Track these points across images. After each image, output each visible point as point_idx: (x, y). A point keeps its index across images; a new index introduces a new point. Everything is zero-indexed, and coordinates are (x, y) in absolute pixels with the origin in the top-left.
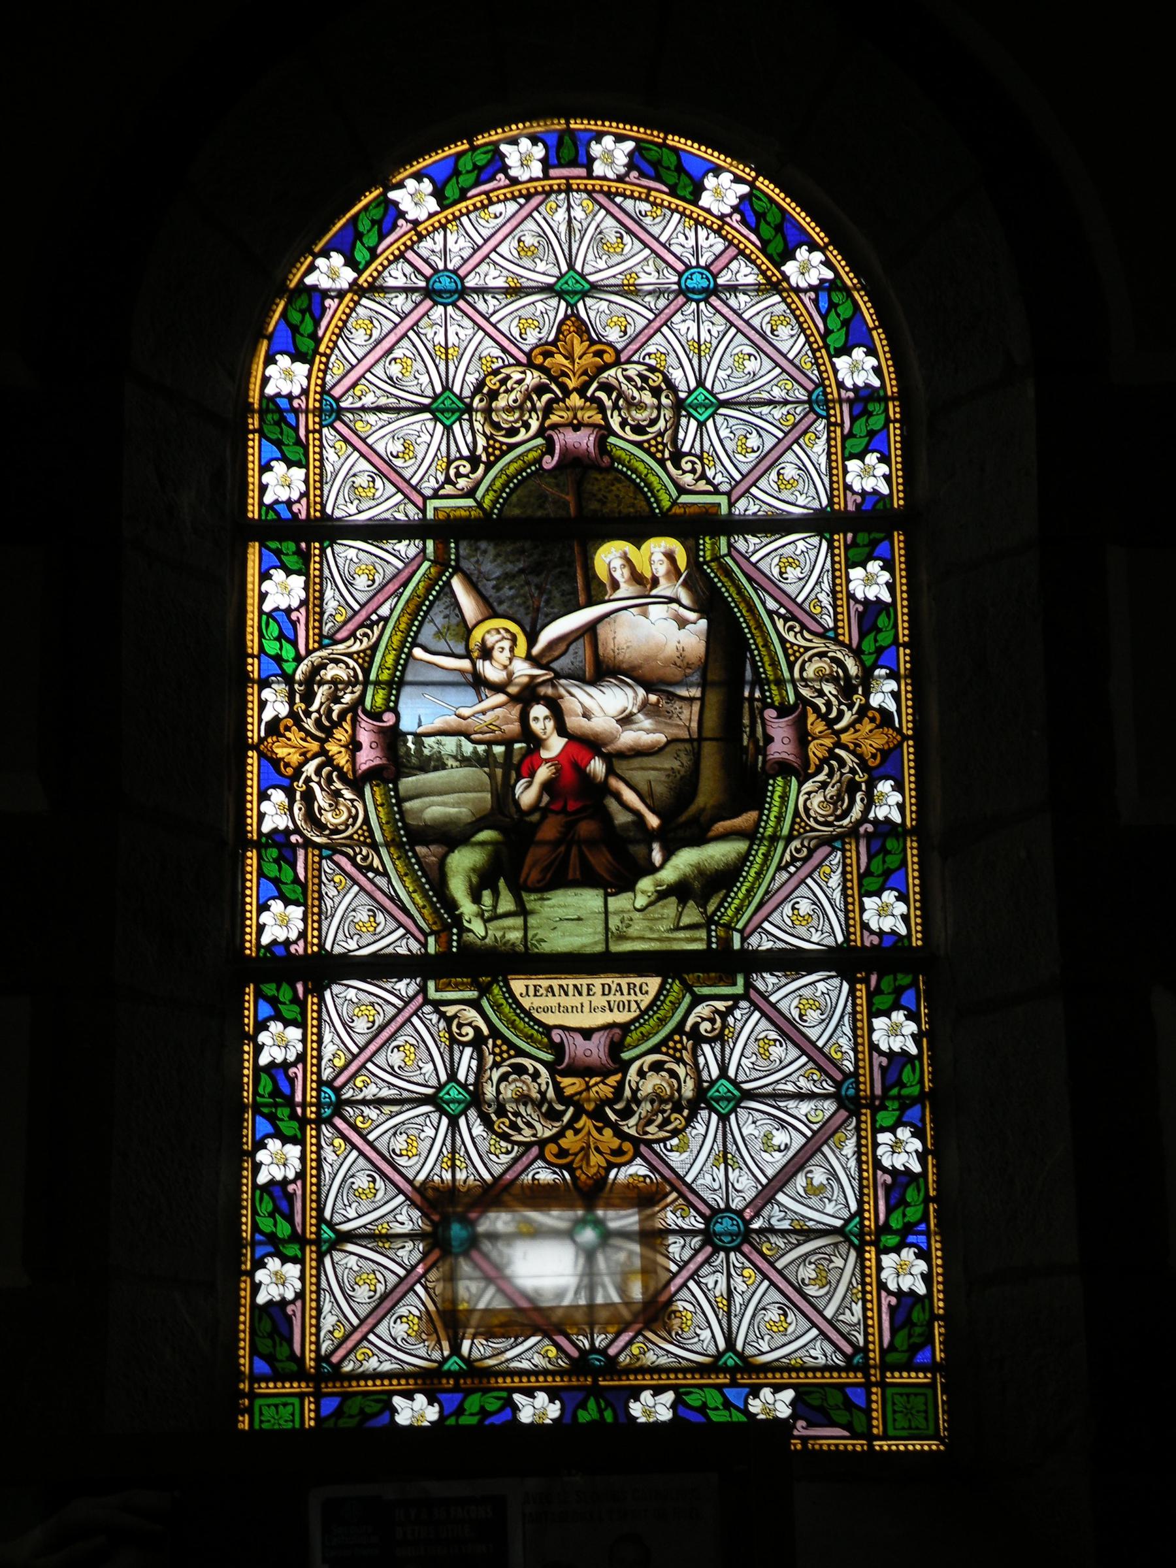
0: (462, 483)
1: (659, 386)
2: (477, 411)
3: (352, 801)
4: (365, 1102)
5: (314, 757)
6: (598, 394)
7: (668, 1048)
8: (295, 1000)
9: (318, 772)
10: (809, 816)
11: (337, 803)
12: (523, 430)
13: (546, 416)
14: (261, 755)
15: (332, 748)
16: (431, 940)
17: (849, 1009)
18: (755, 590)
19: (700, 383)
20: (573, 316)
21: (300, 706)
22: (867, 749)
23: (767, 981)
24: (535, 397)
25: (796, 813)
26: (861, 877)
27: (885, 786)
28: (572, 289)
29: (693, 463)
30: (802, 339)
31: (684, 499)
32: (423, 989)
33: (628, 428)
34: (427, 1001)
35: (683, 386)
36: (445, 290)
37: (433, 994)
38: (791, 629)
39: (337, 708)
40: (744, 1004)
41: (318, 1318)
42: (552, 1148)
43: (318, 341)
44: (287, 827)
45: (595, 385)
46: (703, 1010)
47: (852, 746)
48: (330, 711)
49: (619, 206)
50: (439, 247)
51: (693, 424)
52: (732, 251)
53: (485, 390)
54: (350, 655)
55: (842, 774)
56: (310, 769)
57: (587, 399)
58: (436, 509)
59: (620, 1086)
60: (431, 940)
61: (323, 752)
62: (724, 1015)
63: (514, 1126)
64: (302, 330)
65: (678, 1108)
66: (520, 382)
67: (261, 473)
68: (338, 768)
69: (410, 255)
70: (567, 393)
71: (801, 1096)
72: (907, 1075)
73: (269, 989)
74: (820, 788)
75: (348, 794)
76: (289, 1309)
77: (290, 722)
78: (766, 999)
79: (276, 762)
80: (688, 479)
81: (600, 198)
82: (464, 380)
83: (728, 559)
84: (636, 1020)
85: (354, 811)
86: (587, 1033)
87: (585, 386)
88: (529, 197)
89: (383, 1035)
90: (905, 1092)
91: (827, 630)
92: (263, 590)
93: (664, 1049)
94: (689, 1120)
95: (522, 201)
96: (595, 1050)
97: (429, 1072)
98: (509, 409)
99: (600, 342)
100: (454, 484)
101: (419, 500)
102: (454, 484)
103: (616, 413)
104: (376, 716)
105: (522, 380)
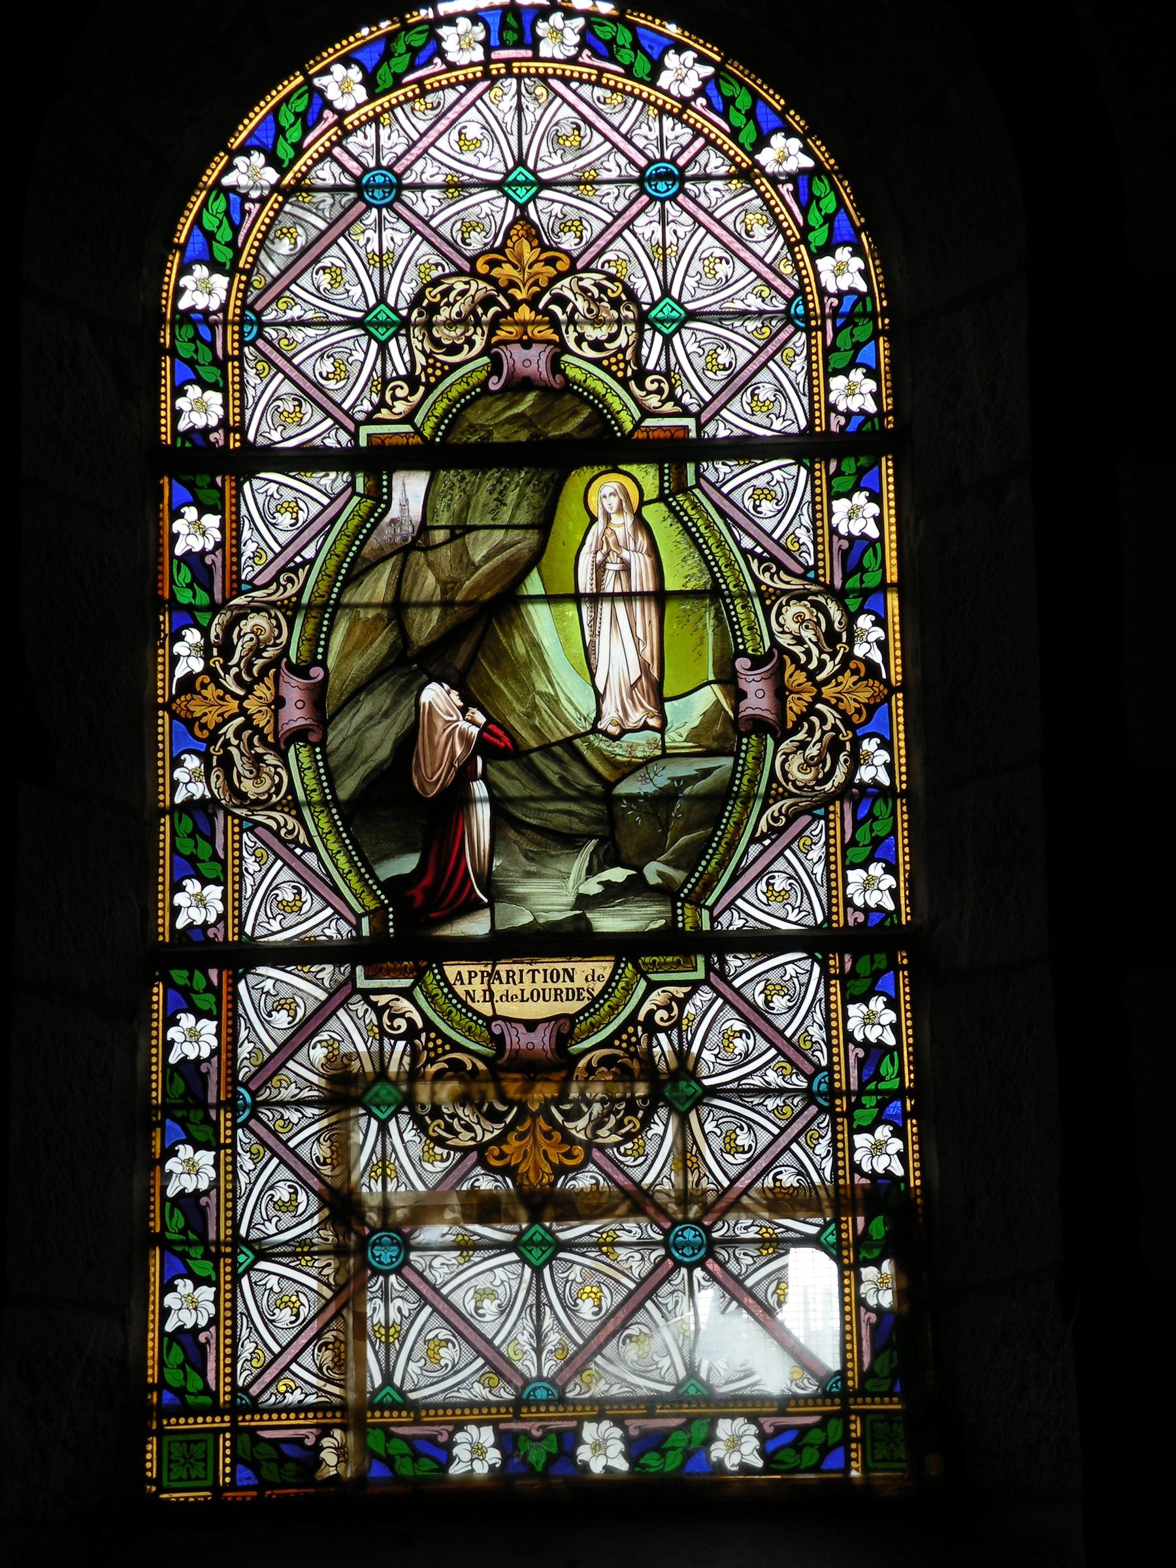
0: (401, 407)
1: (433, 1120)
2: (415, 326)
3: (276, 767)
4: (284, 1104)
5: (233, 717)
6: (504, 1108)
7: (622, 1041)
8: (210, 988)
9: (238, 733)
10: (787, 780)
11: (259, 770)
12: (466, 347)
13: (492, 333)
14: (174, 716)
15: (251, 705)
16: (365, 921)
17: (248, 413)
18: (329, 875)
19: (666, 292)
20: (522, 216)
21: (217, 662)
22: (850, 706)
23: (339, 439)
24: (480, 311)
25: (773, 777)
26: (845, 848)
27: (869, 745)
28: (521, 180)
29: (392, 1027)
30: (781, 240)
31: (649, 422)
32: (700, 427)
33: (585, 345)
34: (697, 416)
35: (646, 298)
36: (380, 189)
37: (690, 423)
38: (767, 569)
39: (260, 662)
40: (360, 417)
41: (234, 1346)
42: (563, 265)
43: (238, 253)
44: (203, 796)
45: (547, 297)
46: (658, 997)
47: (834, 701)
48: (250, 666)
49: (574, 92)
50: (372, 140)
51: (659, 339)
52: (700, 141)
53: (425, 303)
54: (792, 795)
55: (824, 733)
56: (230, 730)
57: (538, 312)
58: (369, 436)
59: (492, 333)
60: (365, 921)
61: (243, 711)
62: (383, 404)
63: (449, 1128)
64: (218, 237)
65: (631, 1110)
66: (463, 293)
67: (174, 398)
68: (258, 730)
69: (337, 151)
70: (515, 304)
71: (301, 323)
72: (887, 1068)
73: (179, 976)
74: (798, 748)
75: (271, 759)
76: (202, 1338)
77: (207, 679)
78: (336, 421)
79: (190, 723)
80: (653, 401)
81: (555, 83)
82: (401, 290)
83: (696, 491)
84: (586, 1009)
85: (277, 779)
86: (531, 1025)
87: (537, 297)
88: (470, 84)
89: (739, 382)
90: (882, 1086)
91: (251, 830)
92: (175, 530)
93: (617, 1043)
94: (646, 1123)
95: (462, 89)
96: (541, 1040)
97: (690, 343)
98: (450, 324)
99: (550, 248)
100: (390, 408)
101: (351, 426)
102: (390, 408)
103: (571, 328)
104: (300, 671)
105: (467, 291)
